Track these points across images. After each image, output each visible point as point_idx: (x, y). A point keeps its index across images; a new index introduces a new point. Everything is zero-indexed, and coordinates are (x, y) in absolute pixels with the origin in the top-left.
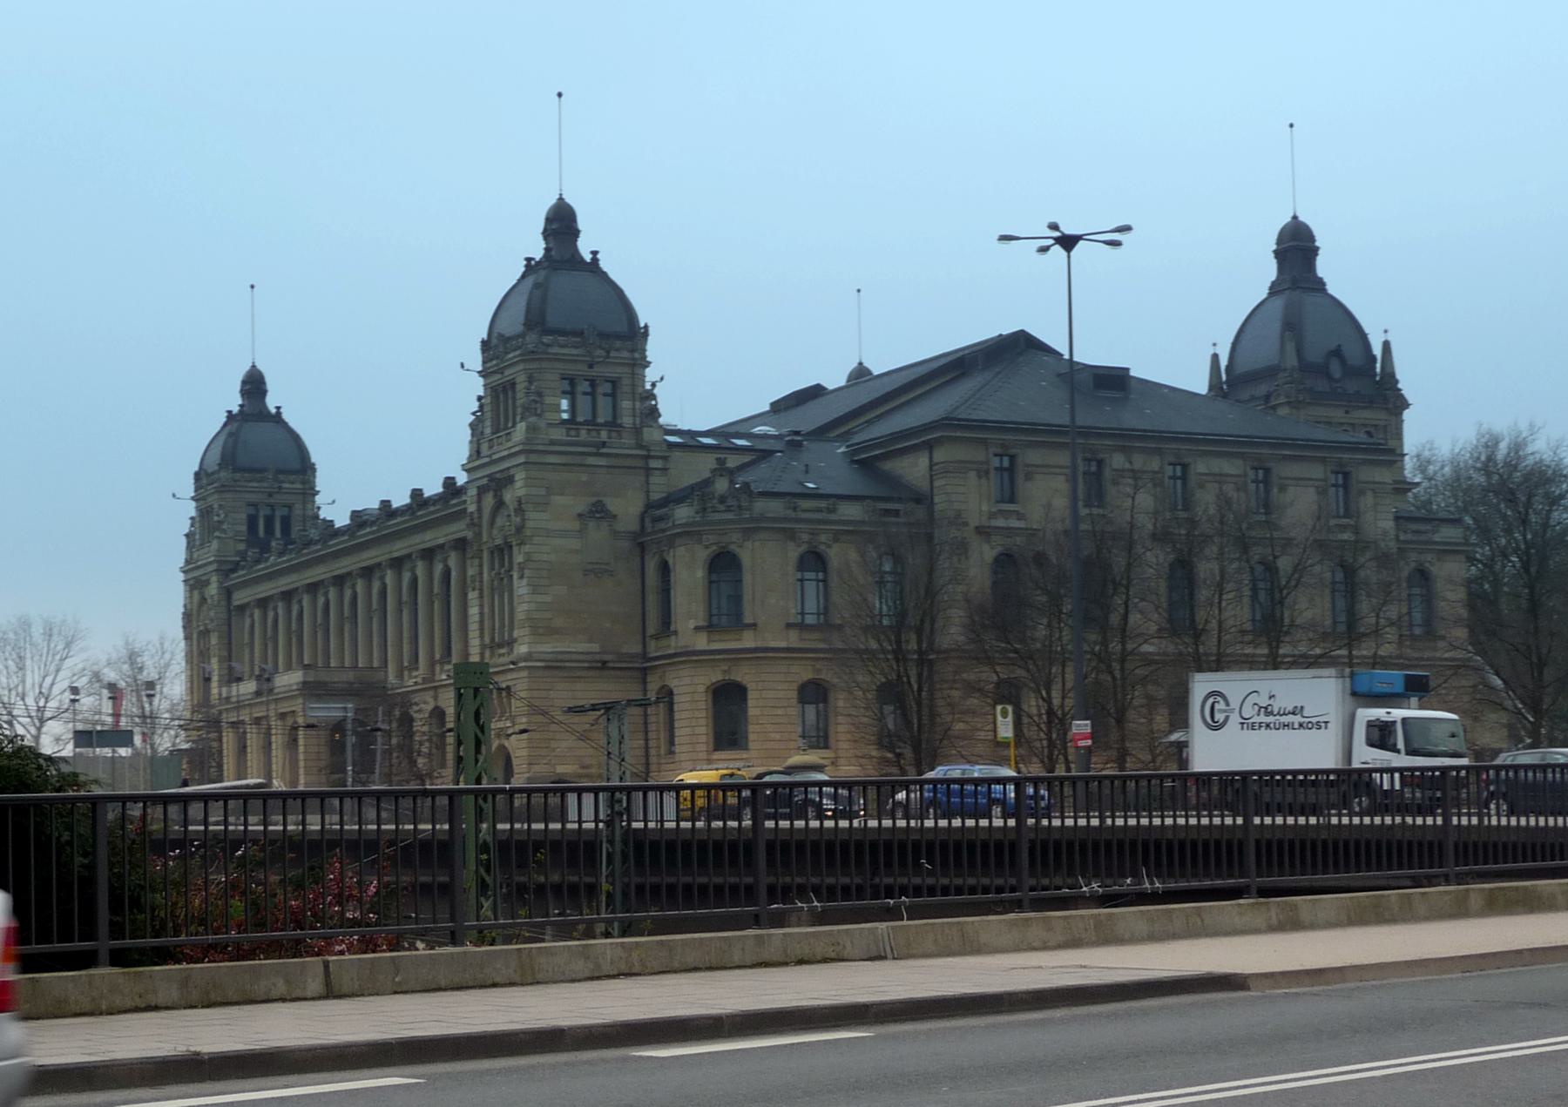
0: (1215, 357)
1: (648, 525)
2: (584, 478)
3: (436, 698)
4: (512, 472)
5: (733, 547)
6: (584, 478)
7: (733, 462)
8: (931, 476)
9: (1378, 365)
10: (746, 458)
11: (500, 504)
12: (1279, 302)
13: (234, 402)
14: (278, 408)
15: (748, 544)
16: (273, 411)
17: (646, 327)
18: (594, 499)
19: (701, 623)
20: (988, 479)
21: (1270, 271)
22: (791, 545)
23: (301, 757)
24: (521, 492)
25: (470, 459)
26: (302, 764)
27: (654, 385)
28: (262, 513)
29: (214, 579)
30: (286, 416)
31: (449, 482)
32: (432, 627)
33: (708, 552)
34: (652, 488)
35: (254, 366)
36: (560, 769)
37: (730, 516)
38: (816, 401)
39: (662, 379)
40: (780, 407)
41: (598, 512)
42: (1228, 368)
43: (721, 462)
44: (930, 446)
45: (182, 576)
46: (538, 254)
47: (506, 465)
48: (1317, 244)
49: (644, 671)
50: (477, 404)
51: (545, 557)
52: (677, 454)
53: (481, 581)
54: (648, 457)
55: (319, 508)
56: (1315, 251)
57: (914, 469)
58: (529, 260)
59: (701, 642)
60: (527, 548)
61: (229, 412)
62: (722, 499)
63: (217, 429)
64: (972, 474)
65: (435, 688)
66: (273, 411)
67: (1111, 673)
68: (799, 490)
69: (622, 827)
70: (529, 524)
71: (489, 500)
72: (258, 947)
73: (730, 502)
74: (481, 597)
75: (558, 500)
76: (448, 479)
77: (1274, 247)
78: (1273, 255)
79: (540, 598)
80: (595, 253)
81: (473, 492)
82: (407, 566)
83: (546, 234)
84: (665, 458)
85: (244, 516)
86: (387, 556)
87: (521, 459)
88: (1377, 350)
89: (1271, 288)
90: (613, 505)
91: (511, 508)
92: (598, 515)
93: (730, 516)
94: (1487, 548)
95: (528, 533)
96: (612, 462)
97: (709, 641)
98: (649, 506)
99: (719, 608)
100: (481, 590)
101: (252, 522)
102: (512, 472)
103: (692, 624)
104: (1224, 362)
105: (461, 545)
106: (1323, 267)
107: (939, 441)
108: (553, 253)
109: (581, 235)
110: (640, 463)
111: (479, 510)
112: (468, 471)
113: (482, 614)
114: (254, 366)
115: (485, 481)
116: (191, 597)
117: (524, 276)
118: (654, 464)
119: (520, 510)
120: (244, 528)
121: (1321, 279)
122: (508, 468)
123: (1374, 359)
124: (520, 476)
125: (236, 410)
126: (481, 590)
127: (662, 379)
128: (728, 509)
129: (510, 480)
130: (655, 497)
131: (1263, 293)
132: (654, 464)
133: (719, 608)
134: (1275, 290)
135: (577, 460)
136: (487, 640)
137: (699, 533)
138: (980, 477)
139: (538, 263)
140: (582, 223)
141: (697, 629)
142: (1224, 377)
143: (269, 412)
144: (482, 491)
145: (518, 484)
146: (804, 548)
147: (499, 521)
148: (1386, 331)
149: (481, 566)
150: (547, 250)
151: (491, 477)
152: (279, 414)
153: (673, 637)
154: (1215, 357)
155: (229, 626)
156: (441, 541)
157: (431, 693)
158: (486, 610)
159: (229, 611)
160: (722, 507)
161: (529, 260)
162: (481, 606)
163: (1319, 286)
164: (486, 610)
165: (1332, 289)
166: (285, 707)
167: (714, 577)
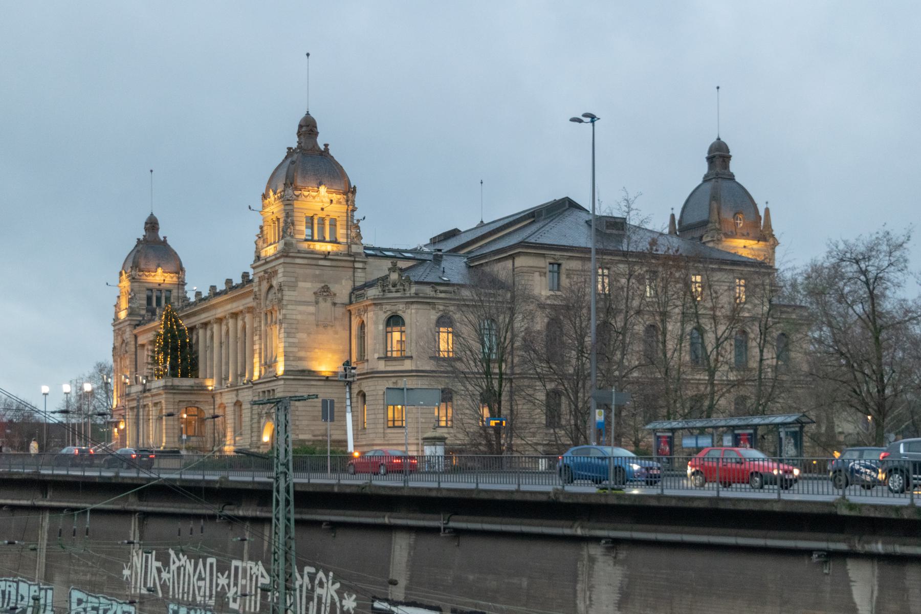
0: (673, 216)
1: (353, 299)
2: (317, 272)
3: (237, 396)
4: (277, 268)
5: (400, 313)
6: (317, 272)
7: (402, 264)
8: (514, 275)
9: (762, 222)
10: (410, 263)
11: (271, 287)
12: (709, 186)
13: (141, 233)
14: (165, 238)
15: (409, 311)
16: (162, 239)
17: (355, 187)
18: (323, 285)
19: (382, 355)
20: (545, 277)
21: (704, 168)
22: (433, 312)
23: (164, 427)
24: (281, 280)
25: (255, 261)
26: (164, 431)
27: (358, 221)
28: (163, 295)
29: (128, 329)
30: (169, 242)
31: (245, 275)
32: (237, 353)
33: (386, 315)
34: (357, 279)
35: (152, 214)
36: (301, 437)
37: (398, 295)
38: (455, 238)
39: (364, 218)
40: (435, 241)
41: (325, 291)
42: (680, 222)
43: (394, 265)
44: (512, 257)
45: (112, 328)
46: (294, 145)
47: (273, 264)
48: (730, 154)
49: (349, 384)
50: (259, 230)
51: (294, 317)
52: (370, 260)
53: (260, 331)
54: (354, 261)
55: (186, 292)
56: (729, 157)
57: (502, 270)
58: (289, 149)
59: (381, 366)
60: (283, 312)
61: (138, 239)
62: (394, 285)
63: (132, 248)
64: (537, 274)
65: (237, 390)
66: (162, 239)
67: (564, 385)
68: (439, 281)
69: (131, 568)
70: (286, 298)
71: (265, 286)
72: (842, 260)
73: (398, 287)
74: (260, 339)
75: (301, 284)
76: (245, 273)
77: (707, 155)
78: (705, 160)
79: (291, 340)
80: (326, 145)
81: (256, 280)
82: (224, 322)
83: (299, 134)
84: (365, 262)
85: (145, 296)
86: (214, 317)
87: (281, 260)
88: (762, 213)
89: (704, 178)
90: (334, 288)
91: (276, 288)
92: (325, 294)
93: (398, 295)
94: (637, 363)
95: (284, 302)
96: (334, 263)
97: (386, 366)
98: (355, 289)
99: (392, 347)
100: (260, 335)
101: (149, 299)
102: (277, 268)
103: (376, 356)
104: (677, 217)
105: (250, 310)
106: (733, 167)
107: (519, 254)
108: (303, 145)
109: (319, 135)
110: (351, 265)
111: (260, 290)
112: (254, 268)
113: (260, 349)
114: (152, 214)
115: (262, 274)
116: (117, 339)
117: (286, 158)
118: (357, 265)
119: (280, 289)
120: (145, 302)
121: (732, 174)
122: (275, 266)
123: (760, 217)
124: (281, 270)
125: (141, 238)
126: (260, 335)
127: (364, 218)
128: (397, 291)
129: (276, 272)
130: (358, 284)
131: (700, 181)
132: (357, 265)
133: (392, 347)
134: (706, 179)
135: (314, 262)
136: (263, 362)
137: (380, 304)
138: (541, 276)
139: (294, 151)
140: (320, 129)
141: (379, 358)
142: (677, 227)
143: (160, 239)
144: (261, 279)
145: (280, 275)
146: (440, 314)
147: (270, 296)
148: (767, 203)
149: (260, 322)
150: (299, 143)
151: (265, 272)
152: (165, 241)
153: (366, 364)
154: (673, 216)
155: (136, 355)
156: (241, 308)
157: (235, 392)
158: (263, 347)
159: (136, 348)
160: (393, 289)
161: (289, 149)
162: (260, 344)
163: (731, 177)
164: (263, 347)
165: (738, 179)
166: (156, 399)
167: (389, 329)
